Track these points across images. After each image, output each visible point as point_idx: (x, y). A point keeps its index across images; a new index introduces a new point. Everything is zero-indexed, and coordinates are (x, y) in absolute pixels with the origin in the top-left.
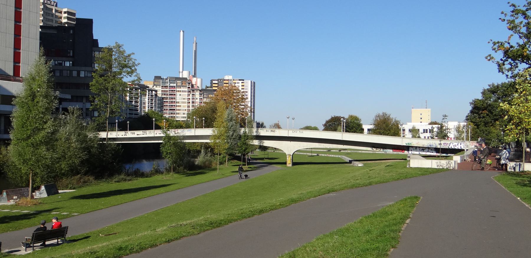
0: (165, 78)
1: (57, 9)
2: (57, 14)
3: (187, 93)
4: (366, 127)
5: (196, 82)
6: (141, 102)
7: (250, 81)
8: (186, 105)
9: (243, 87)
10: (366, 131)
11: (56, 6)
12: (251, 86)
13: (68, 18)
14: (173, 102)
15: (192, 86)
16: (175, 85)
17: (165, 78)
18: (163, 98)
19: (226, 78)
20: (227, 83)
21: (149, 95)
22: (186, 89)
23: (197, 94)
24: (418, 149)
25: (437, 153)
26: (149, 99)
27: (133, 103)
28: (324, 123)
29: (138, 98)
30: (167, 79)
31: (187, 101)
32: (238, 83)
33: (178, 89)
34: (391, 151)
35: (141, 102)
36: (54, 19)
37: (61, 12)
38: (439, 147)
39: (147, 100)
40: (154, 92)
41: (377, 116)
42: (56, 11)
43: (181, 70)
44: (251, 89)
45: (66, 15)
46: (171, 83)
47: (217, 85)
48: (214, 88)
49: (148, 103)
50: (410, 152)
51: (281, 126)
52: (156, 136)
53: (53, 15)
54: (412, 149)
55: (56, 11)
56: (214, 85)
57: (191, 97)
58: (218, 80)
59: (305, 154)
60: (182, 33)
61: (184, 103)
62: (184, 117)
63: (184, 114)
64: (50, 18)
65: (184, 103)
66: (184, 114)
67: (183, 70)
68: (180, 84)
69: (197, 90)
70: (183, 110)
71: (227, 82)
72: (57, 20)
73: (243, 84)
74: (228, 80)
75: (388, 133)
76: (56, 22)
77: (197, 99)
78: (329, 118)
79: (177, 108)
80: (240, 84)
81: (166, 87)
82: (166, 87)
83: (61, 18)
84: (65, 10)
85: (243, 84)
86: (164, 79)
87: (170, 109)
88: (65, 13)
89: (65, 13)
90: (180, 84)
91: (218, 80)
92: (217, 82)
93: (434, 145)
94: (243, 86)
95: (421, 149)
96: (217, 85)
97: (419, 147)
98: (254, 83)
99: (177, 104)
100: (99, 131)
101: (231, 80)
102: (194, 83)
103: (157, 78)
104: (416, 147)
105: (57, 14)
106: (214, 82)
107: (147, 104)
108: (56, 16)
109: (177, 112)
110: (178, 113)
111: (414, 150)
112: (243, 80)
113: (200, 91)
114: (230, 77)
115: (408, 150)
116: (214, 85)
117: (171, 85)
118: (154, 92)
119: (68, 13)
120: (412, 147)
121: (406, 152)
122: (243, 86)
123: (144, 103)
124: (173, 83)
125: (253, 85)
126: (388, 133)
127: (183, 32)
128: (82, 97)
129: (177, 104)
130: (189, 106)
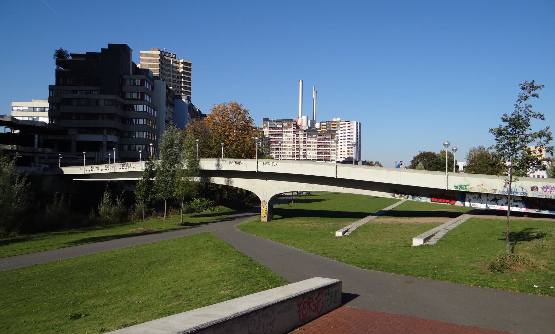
1: (175, 60)
2: (175, 65)
3: (292, 134)
4: (461, 164)
5: (302, 123)
7: (355, 123)
8: (292, 144)
10: (461, 168)
11: (175, 58)
12: (357, 127)
13: (184, 68)
15: (298, 127)
16: (281, 126)
19: (335, 120)
22: (292, 130)
23: (302, 134)
24: (484, 198)
25: (527, 207)
28: (412, 159)
30: (274, 121)
32: (345, 124)
33: (284, 130)
34: (428, 200)
36: (172, 69)
37: (179, 63)
38: (531, 194)
41: (471, 151)
42: (174, 62)
43: (300, 116)
44: (357, 130)
45: (182, 65)
47: (325, 127)
48: (322, 130)
50: (467, 204)
51: (382, 164)
52: (117, 171)
53: (170, 65)
54: (471, 197)
55: (174, 62)
56: (322, 127)
57: (296, 137)
58: (326, 122)
60: (301, 82)
61: (290, 142)
63: (289, 153)
64: (168, 68)
65: (290, 142)
66: (289, 153)
68: (286, 126)
69: (302, 130)
70: (289, 149)
71: (335, 123)
72: (175, 70)
74: (335, 122)
75: (485, 171)
76: (174, 72)
78: (418, 153)
80: (347, 125)
83: (178, 68)
84: (182, 61)
88: (182, 63)
89: (182, 63)
91: (326, 122)
92: (325, 124)
93: (519, 190)
94: (349, 127)
95: (492, 198)
96: (325, 127)
97: (487, 195)
98: (360, 124)
101: (338, 122)
102: (299, 124)
103: (266, 120)
104: (480, 195)
105: (175, 65)
106: (322, 124)
110: (284, 153)
111: (475, 200)
112: (349, 121)
113: (304, 131)
114: (339, 119)
115: (463, 200)
116: (322, 127)
119: (184, 63)
120: (472, 193)
121: (458, 203)
122: (349, 127)
125: (359, 126)
126: (485, 171)
127: (302, 81)
128: (103, 128)
130: (294, 146)
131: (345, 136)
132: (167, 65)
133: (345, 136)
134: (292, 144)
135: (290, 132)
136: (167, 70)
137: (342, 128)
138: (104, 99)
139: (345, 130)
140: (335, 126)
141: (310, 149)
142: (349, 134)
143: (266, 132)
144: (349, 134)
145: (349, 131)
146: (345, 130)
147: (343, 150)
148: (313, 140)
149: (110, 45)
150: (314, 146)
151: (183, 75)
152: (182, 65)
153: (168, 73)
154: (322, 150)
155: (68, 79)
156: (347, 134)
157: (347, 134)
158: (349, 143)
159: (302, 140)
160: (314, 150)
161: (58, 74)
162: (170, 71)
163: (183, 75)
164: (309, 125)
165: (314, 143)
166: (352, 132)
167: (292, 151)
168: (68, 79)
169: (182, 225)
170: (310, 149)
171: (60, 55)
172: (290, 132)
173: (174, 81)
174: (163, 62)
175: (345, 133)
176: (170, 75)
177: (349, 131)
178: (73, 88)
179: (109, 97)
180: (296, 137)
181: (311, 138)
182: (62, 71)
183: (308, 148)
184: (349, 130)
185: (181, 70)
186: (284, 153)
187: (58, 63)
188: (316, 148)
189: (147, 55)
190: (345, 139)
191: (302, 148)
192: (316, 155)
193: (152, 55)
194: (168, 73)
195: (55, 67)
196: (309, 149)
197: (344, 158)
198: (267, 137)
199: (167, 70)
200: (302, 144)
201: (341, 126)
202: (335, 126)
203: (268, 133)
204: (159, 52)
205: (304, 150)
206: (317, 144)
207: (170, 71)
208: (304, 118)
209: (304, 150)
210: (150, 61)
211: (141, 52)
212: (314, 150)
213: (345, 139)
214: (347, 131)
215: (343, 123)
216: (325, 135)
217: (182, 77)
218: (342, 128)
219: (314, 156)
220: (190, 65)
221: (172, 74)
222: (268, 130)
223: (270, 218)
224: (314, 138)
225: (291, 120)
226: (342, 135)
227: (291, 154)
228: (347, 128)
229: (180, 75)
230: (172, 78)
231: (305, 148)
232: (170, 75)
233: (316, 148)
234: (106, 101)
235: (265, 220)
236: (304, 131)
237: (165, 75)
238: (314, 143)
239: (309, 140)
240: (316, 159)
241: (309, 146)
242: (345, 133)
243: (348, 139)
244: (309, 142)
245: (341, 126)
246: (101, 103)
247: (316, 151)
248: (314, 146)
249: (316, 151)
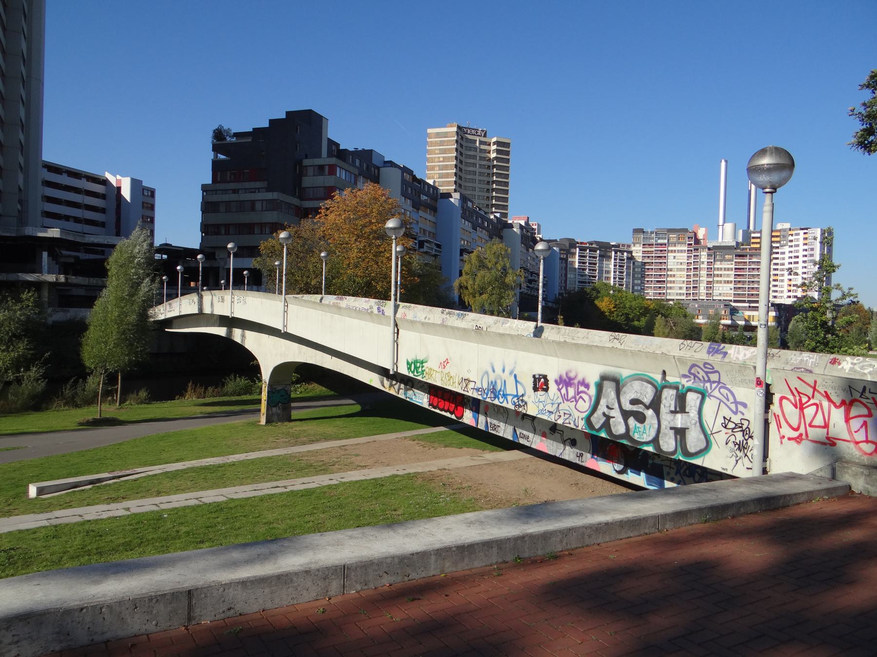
0: (649, 230)
1: (483, 139)
2: (483, 147)
3: (686, 254)
6: (601, 272)
8: (685, 273)
9: (806, 242)
11: (485, 136)
13: (498, 151)
14: (663, 269)
15: (697, 241)
16: (666, 241)
17: (649, 230)
18: (645, 263)
20: (777, 236)
21: (615, 259)
22: (686, 248)
23: (704, 255)
26: (615, 266)
27: (587, 272)
29: (595, 264)
30: (652, 233)
31: (685, 267)
32: (797, 234)
33: (670, 248)
35: (601, 272)
36: (478, 154)
37: (489, 145)
39: (612, 267)
40: (625, 254)
42: (481, 143)
43: (721, 222)
45: (495, 147)
46: (659, 238)
49: (615, 272)
55: (481, 143)
59: (266, 488)
60: (723, 164)
61: (681, 270)
62: (680, 294)
63: (681, 288)
64: (472, 153)
65: (681, 270)
66: (681, 288)
67: (724, 222)
68: (675, 240)
70: (679, 282)
71: (778, 234)
72: (483, 155)
73: (806, 236)
74: (780, 231)
76: (482, 159)
77: (703, 263)
79: (669, 279)
80: (802, 236)
81: (651, 245)
82: (651, 245)
83: (489, 152)
84: (494, 140)
85: (806, 236)
86: (647, 232)
87: (658, 281)
89: (494, 143)
90: (675, 240)
99: (669, 273)
100: (603, 313)
101: (785, 230)
103: (637, 231)
105: (483, 147)
107: (612, 273)
108: (482, 151)
109: (669, 285)
110: (671, 288)
112: (807, 229)
114: (787, 226)
117: (660, 241)
118: (625, 254)
119: (498, 143)
123: (608, 272)
124: (662, 238)
125: (827, 240)
127: (726, 161)
129: (669, 273)
131: (798, 257)
132: (470, 149)
133: (798, 257)
134: (685, 273)
135: (681, 251)
136: (470, 157)
137: (791, 241)
138: (263, 200)
139: (797, 246)
140: (778, 239)
141: (721, 282)
142: (805, 253)
143: (638, 252)
144: (805, 253)
145: (806, 247)
146: (797, 246)
147: (792, 283)
148: (725, 265)
149: (288, 113)
150: (728, 275)
151: (495, 163)
152: (495, 147)
153: (472, 161)
154: (744, 282)
155: (229, 173)
156: (801, 254)
157: (801, 254)
158: (805, 270)
159: (705, 266)
160: (728, 282)
161: (217, 166)
162: (474, 157)
163: (495, 163)
164: (740, 240)
165: (728, 269)
166: (812, 249)
167: (684, 285)
168: (229, 173)
169: (81, 424)
170: (721, 282)
171: (219, 135)
172: (681, 251)
173: (481, 174)
174: (464, 144)
175: (797, 251)
176: (474, 165)
177: (806, 247)
178: (233, 186)
179: (270, 196)
180: (692, 260)
181: (721, 261)
182: (222, 161)
183: (716, 279)
184: (805, 244)
185: (493, 155)
186: (671, 288)
187: (216, 149)
188: (732, 279)
189: (438, 135)
190: (797, 263)
191: (704, 279)
192: (732, 292)
193: (446, 135)
194: (472, 161)
195: (211, 155)
196: (718, 282)
197: (796, 297)
198: (640, 260)
199: (470, 157)
200: (704, 273)
201: (790, 238)
202: (778, 239)
203: (641, 254)
204: (455, 129)
205: (709, 282)
206: (733, 273)
207: (474, 157)
208: (729, 227)
209: (709, 282)
210: (442, 143)
211: (429, 131)
212: (728, 282)
213: (797, 263)
214: (802, 247)
215: (793, 232)
216: (751, 256)
217: (494, 166)
218: (791, 241)
219: (727, 295)
220: (507, 145)
221: (478, 162)
222: (641, 248)
223: (268, 421)
224: (729, 260)
225: (686, 230)
226: (793, 255)
227: (684, 291)
228: (801, 242)
229: (491, 164)
230: (477, 169)
231: (711, 279)
232: (474, 165)
233: (732, 279)
234: (264, 203)
235: (263, 421)
236: (709, 249)
237: (467, 164)
238: (728, 269)
239: (718, 265)
240: (732, 298)
241: (718, 276)
242: (797, 251)
243: (804, 262)
244: (718, 269)
245: (790, 238)
246: (258, 206)
247: (732, 286)
248: (728, 275)
249: (732, 286)
